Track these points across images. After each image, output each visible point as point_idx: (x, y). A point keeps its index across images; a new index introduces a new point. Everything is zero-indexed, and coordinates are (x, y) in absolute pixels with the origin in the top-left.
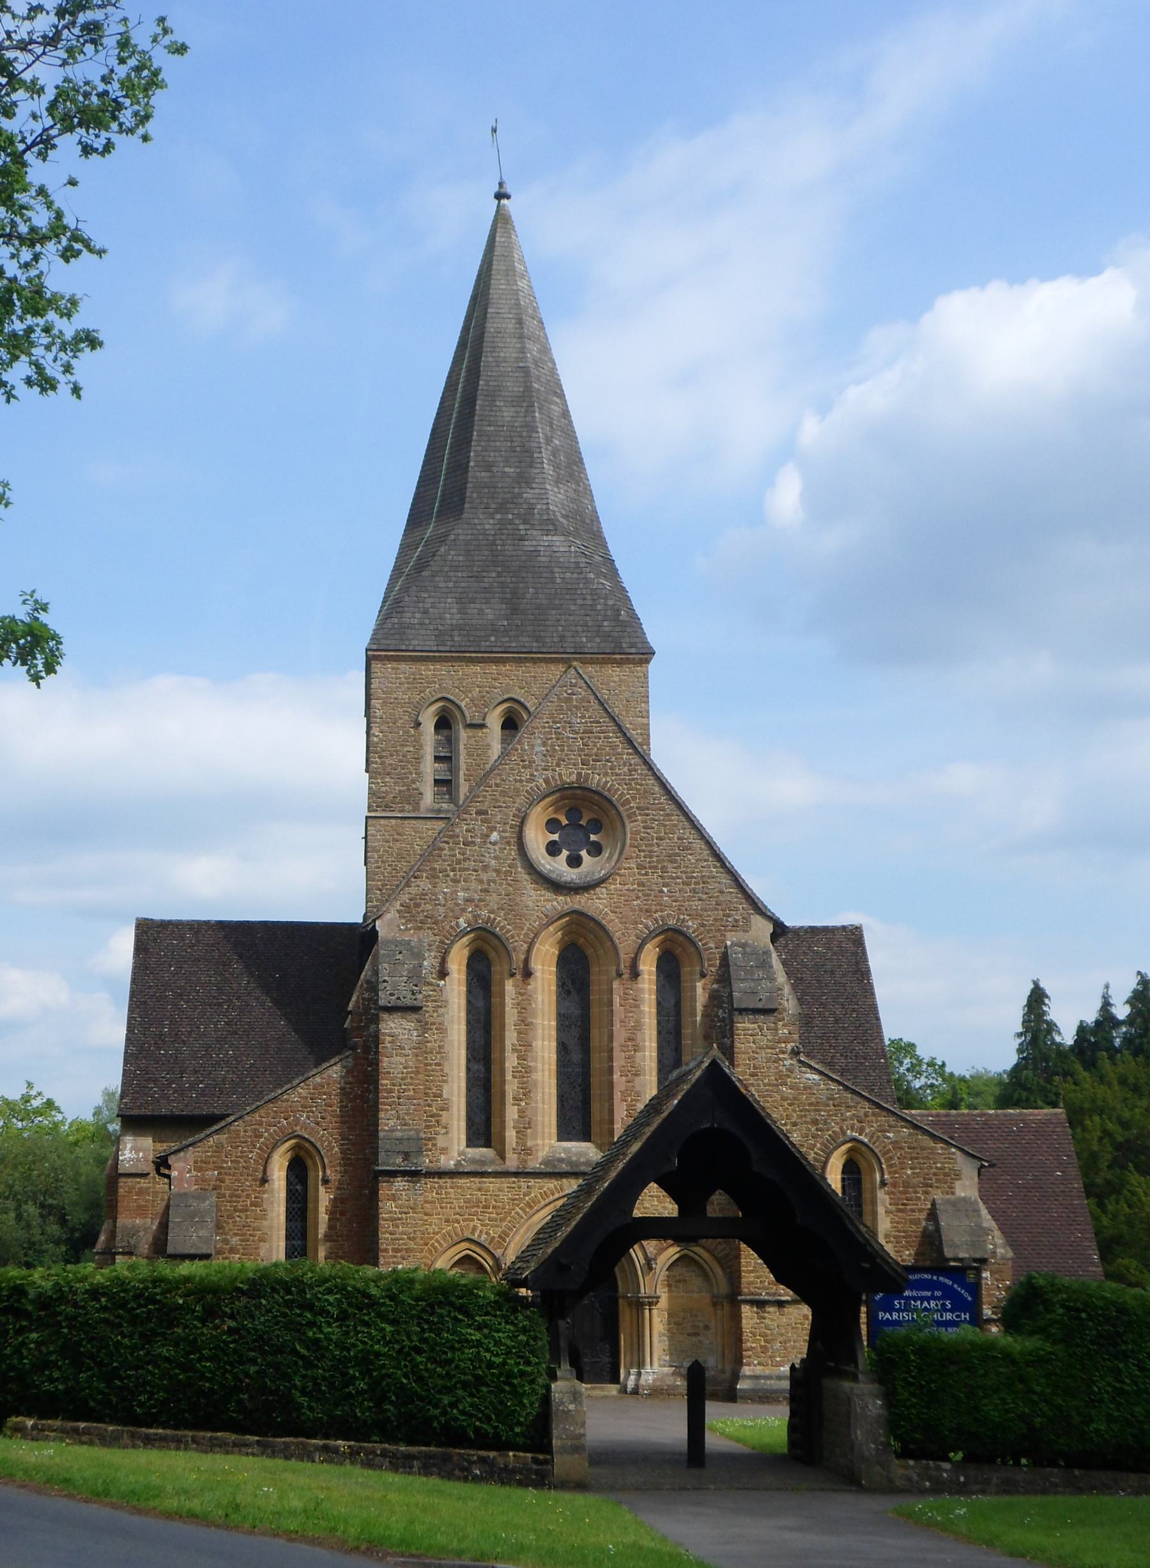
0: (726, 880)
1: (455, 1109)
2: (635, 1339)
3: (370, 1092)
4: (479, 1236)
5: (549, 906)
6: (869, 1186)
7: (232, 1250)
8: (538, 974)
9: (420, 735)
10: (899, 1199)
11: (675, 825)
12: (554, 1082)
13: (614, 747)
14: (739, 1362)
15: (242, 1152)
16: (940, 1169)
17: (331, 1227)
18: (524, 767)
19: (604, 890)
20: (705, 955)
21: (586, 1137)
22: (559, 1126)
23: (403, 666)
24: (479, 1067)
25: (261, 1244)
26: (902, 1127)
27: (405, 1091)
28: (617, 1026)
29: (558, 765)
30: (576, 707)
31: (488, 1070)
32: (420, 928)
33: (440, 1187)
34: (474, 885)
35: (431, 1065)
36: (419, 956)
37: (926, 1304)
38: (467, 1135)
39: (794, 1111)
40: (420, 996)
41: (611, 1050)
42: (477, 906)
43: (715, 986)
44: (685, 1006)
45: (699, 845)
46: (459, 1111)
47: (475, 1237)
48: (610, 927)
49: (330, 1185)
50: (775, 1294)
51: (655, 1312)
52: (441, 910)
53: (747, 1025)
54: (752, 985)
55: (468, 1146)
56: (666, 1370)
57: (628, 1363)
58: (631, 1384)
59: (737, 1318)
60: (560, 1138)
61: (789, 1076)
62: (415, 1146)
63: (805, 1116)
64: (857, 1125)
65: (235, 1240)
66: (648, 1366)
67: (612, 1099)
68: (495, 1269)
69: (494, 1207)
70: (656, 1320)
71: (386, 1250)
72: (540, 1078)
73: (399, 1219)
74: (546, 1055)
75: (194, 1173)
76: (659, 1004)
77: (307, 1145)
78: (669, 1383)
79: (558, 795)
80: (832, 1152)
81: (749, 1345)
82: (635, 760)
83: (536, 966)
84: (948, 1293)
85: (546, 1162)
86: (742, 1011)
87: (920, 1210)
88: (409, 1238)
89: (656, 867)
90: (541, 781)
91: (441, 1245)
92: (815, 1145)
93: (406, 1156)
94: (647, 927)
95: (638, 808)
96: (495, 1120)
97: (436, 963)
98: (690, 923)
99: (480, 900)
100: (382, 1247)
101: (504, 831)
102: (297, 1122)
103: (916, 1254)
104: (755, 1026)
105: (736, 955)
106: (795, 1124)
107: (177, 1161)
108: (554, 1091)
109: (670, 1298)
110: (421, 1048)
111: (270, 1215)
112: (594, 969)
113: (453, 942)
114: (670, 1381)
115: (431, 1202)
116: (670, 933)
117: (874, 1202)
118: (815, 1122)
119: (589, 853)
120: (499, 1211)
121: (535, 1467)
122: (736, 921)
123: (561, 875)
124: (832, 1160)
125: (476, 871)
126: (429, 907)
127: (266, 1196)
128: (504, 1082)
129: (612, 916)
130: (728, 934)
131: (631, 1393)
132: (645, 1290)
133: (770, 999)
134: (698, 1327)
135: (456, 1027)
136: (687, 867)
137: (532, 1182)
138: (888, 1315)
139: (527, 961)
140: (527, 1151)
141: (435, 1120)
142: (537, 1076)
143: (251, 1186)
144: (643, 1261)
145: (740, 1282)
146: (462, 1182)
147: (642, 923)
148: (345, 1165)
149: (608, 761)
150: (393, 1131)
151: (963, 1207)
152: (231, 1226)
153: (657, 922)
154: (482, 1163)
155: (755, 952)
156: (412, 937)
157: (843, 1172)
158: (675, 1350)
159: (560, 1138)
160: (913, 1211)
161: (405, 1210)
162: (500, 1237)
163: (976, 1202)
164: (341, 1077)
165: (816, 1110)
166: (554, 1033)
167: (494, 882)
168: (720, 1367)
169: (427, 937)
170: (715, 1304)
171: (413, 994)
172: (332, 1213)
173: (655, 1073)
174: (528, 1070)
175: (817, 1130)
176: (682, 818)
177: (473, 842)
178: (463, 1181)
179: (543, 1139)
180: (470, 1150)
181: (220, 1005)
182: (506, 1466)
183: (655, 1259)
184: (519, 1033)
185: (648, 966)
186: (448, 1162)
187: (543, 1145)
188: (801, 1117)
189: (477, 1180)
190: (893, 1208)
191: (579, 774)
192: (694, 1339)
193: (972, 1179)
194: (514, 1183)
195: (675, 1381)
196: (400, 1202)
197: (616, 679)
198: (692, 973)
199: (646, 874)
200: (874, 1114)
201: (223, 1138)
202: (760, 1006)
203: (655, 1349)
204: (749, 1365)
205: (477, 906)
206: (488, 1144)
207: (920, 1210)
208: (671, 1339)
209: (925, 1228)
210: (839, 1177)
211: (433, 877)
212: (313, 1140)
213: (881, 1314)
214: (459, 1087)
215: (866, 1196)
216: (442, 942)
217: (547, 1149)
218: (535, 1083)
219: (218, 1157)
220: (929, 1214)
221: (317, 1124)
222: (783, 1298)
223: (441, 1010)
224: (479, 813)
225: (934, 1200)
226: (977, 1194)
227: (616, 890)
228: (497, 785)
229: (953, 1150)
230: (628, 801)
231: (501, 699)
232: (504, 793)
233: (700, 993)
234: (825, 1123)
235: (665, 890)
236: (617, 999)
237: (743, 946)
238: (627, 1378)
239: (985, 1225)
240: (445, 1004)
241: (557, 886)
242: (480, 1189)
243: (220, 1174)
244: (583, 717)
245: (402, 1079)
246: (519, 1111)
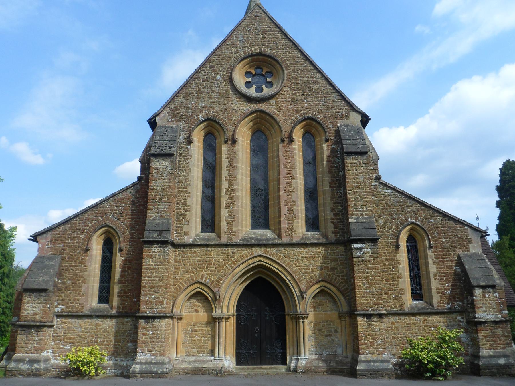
0: (336, 96)
1: (193, 211)
2: (295, 339)
4: (205, 281)
5: (245, 109)
6: (422, 249)
7: (67, 288)
10: (440, 255)
12: (249, 198)
13: (277, 38)
14: (357, 351)
15: (77, 234)
16: (460, 238)
17: (122, 276)
18: (233, 47)
19: (274, 101)
20: (327, 130)
21: (267, 226)
22: (252, 222)
24: (209, 192)
25: (83, 285)
26: (438, 216)
27: (163, 198)
28: (282, 167)
29: (250, 46)
30: (259, 21)
31: (214, 192)
33: (184, 253)
34: (207, 100)
35: (181, 188)
38: (202, 226)
39: (379, 209)
41: (279, 180)
42: (208, 110)
43: (333, 146)
44: (318, 157)
45: (321, 80)
46: (196, 212)
47: (203, 281)
48: (277, 118)
49: (123, 252)
50: (377, 310)
51: (306, 323)
52: (190, 111)
53: (352, 161)
54: (353, 141)
55: (202, 232)
56: (313, 357)
57: (291, 352)
58: (293, 366)
59: (355, 325)
60: (253, 228)
62: (165, 228)
63: (385, 212)
64: (414, 216)
65: (68, 283)
66: (303, 355)
67: (280, 204)
68: (214, 299)
69: (214, 264)
70: (307, 327)
71: (145, 287)
72: (240, 194)
73: (154, 269)
74: (244, 183)
75: (50, 246)
77: (112, 231)
78: (315, 365)
79: (250, 59)
80: (401, 231)
81: (363, 341)
82: (289, 43)
83: (238, 137)
85: (243, 239)
86: (349, 153)
87: (452, 261)
88: (159, 280)
89: (300, 90)
90: (242, 53)
91: (183, 286)
92: (392, 227)
93: (160, 233)
94: (296, 118)
95: (290, 64)
96: (216, 218)
97: (186, 137)
98: (319, 116)
99: (210, 107)
100: (143, 285)
101: (222, 75)
102: (107, 218)
103: (452, 285)
104: (357, 161)
105: (343, 130)
106: (380, 216)
107: (41, 239)
108: (249, 203)
109: (315, 315)
111: (89, 268)
112: (270, 141)
114: (315, 363)
115: (178, 262)
116: (308, 121)
117: (426, 257)
118: (391, 215)
119: (266, 87)
120: (217, 266)
122: (342, 114)
124: (402, 235)
127: (87, 258)
128: (220, 197)
129: (278, 113)
130: (339, 121)
131: (293, 371)
132: (300, 310)
133: (363, 147)
134: (331, 331)
135: (196, 169)
136: (316, 90)
137: (235, 250)
139: (233, 135)
140: (233, 233)
142: (239, 193)
143: (80, 253)
144: (298, 294)
145: (356, 304)
146: (196, 250)
147: (294, 116)
148: (132, 241)
149: (275, 44)
150: (154, 220)
153: (302, 116)
154: (208, 240)
155: (353, 128)
156: (174, 124)
157: (407, 242)
158: (319, 345)
159: (253, 228)
160: (448, 261)
161: (158, 264)
162: (217, 281)
163: (481, 256)
164: (133, 195)
165: (391, 208)
166: (249, 173)
167: (218, 98)
168: (345, 354)
169: (182, 124)
170: (340, 318)
171: (170, 148)
172: (124, 268)
173: (303, 192)
174: (234, 190)
175: (392, 219)
176: (313, 68)
177: (207, 80)
178: (197, 250)
179: (242, 227)
180: (202, 234)
183: (305, 292)
184: (229, 171)
185: (298, 135)
186: (189, 240)
187: (242, 230)
188: (383, 212)
189: (205, 249)
190: (437, 260)
192: (329, 338)
193: (478, 243)
194: (225, 251)
195: (318, 363)
196: (155, 259)
198: (320, 141)
199: (295, 94)
200: (422, 210)
202: (358, 150)
203: (307, 344)
204: (363, 354)
205: (208, 110)
206: (213, 231)
207: (452, 261)
208: (316, 338)
209: (456, 271)
210: (405, 244)
211: (186, 96)
212: (115, 228)
214: (197, 200)
215: (421, 254)
216: (190, 127)
217: (244, 233)
218: (238, 197)
219: (64, 237)
220: (457, 263)
221: (118, 219)
222: (382, 312)
223: (188, 161)
224: (210, 67)
225: (459, 255)
226: (481, 251)
228: (220, 55)
229: (466, 227)
230: (285, 61)
233: (326, 150)
234: (396, 215)
235: (305, 100)
236: (281, 154)
237: (347, 126)
238: (290, 362)
240: (190, 157)
241: (250, 99)
242: (206, 254)
243: (64, 246)
244: (262, 25)
246: (229, 212)
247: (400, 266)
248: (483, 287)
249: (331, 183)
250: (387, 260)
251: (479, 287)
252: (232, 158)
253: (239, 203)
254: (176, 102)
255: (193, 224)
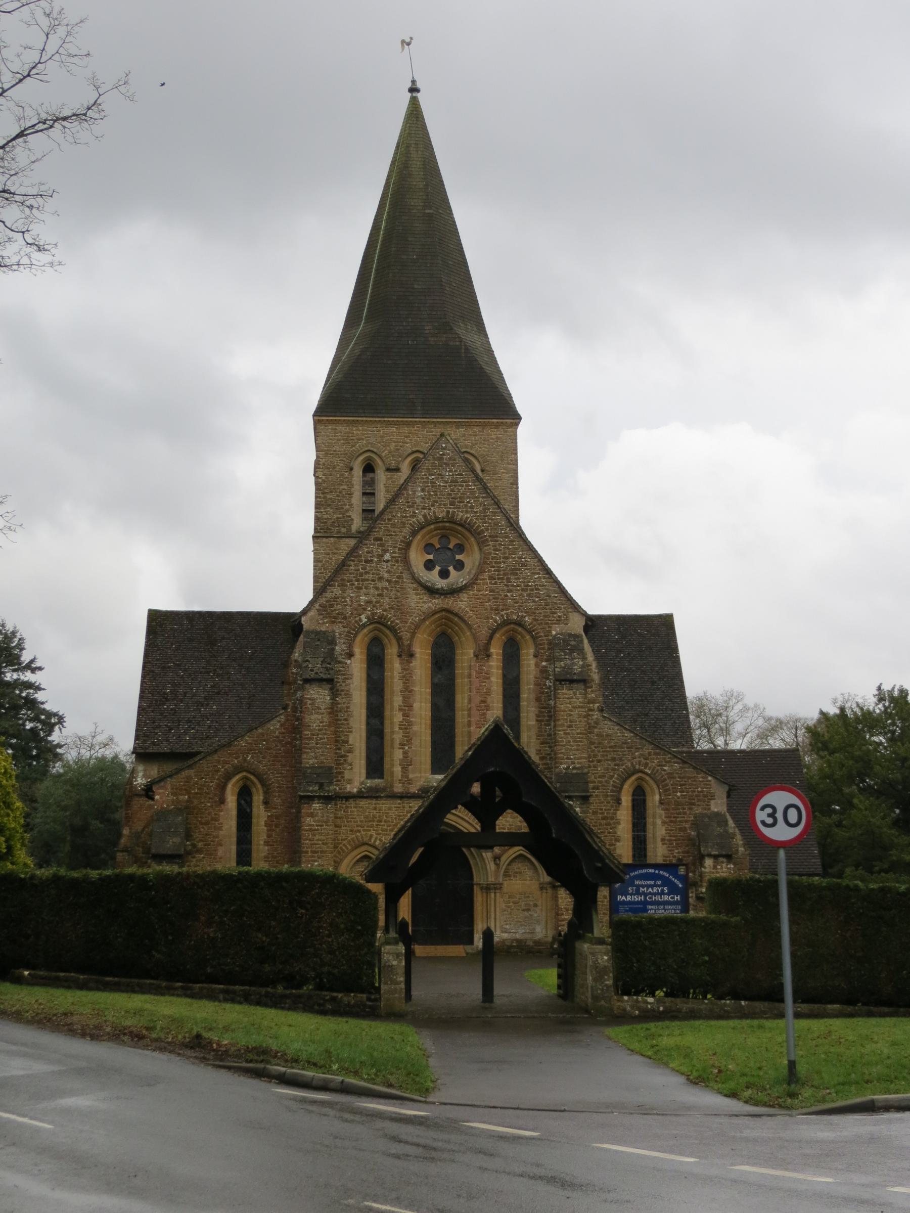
3: (297, 740)
4: (375, 841)
8: (418, 655)
9: (352, 476)
11: (517, 549)
12: (429, 732)
18: (408, 507)
23: (339, 428)
25: (219, 848)
27: (321, 739)
29: (433, 505)
30: (446, 464)
32: (333, 622)
33: (347, 807)
36: (333, 642)
37: (650, 890)
40: (331, 672)
55: (367, 778)
61: (595, 727)
64: (643, 761)
69: (385, 821)
71: (307, 852)
73: (317, 830)
74: (423, 713)
76: (504, 676)
84: (666, 882)
87: (686, 821)
89: (502, 579)
94: (496, 621)
95: (490, 536)
99: (377, 602)
101: (394, 552)
104: (571, 692)
108: (429, 738)
110: (333, 710)
112: (458, 652)
113: (357, 634)
118: (613, 759)
119: (455, 568)
121: (369, 1003)
122: (560, 617)
123: (434, 584)
125: (373, 581)
126: (340, 607)
129: (471, 613)
134: (530, 905)
138: (624, 898)
139: (410, 646)
140: (410, 781)
141: (341, 759)
151: (719, 818)
152: (197, 835)
160: (681, 822)
166: (429, 697)
167: (386, 588)
170: (541, 889)
174: (410, 724)
181: (208, 673)
182: (349, 1003)
184: (404, 697)
190: (667, 820)
191: (448, 512)
192: (526, 913)
197: (494, 437)
199: (495, 583)
200: (656, 754)
201: (191, 772)
206: (381, 776)
207: (686, 821)
211: (342, 585)
213: (619, 897)
217: (423, 780)
223: (348, 682)
227: (474, 595)
228: (389, 520)
230: (483, 532)
231: (410, 451)
232: (394, 525)
234: (621, 760)
235: (509, 594)
239: (731, 831)
242: (375, 809)
245: (320, 730)
247: (620, 827)
248: (716, 857)
249: (538, 716)
250: (603, 819)
251: (710, 856)
252: (407, 678)
253: (416, 742)
254: (328, 595)
255: (356, 769)
